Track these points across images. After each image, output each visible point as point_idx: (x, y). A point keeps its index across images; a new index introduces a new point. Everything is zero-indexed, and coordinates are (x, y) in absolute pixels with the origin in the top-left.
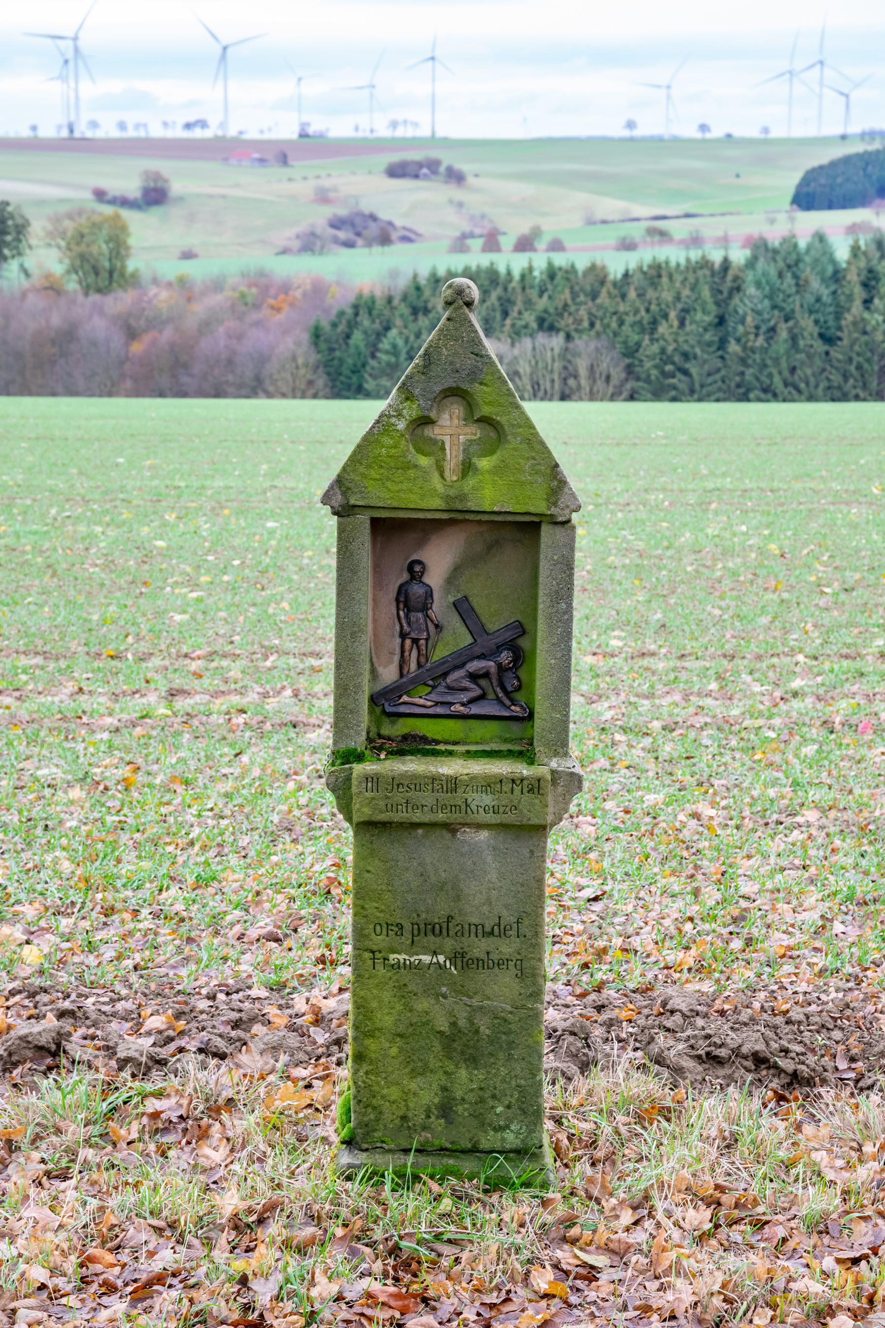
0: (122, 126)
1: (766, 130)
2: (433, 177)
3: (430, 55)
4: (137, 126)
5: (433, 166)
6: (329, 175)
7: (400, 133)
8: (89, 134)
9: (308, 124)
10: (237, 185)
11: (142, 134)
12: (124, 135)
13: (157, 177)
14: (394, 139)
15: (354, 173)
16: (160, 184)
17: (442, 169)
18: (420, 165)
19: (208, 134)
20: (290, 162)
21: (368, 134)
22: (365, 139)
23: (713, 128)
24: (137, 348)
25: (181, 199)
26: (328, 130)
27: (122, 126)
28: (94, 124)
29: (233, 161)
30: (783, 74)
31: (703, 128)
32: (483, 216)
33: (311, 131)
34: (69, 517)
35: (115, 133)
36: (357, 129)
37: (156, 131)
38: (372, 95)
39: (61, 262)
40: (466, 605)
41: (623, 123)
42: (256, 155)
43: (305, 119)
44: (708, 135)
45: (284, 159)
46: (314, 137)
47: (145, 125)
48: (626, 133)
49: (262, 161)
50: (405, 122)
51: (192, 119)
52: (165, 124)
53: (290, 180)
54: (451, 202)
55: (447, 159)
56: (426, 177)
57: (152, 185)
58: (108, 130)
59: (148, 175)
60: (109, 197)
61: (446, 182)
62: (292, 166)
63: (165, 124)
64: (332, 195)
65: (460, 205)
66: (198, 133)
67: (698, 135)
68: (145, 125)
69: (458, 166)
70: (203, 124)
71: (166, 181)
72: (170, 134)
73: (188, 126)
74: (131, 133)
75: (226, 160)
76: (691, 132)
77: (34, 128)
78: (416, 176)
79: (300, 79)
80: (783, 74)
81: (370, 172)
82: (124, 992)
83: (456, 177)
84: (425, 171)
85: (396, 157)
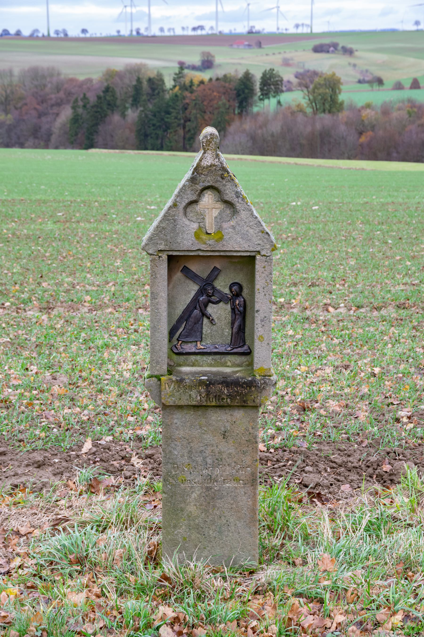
0: (162, 30)
1: (118, 32)
2: (336, 52)
4: (169, 30)
5: (335, 46)
6: (285, 52)
7: (300, 30)
8: (145, 34)
9: (254, 27)
10: (243, 58)
11: (172, 34)
12: (163, 34)
13: (208, 54)
14: (297, 34)
15: (296, 51)
16: (210, 58)
17: (339, 48)
18: (329, 46)
19: (204, 32)
20: (263, 46)
21: (284, 32)
22: (282, 34)
23: (89, 30)
24: (363, 139)
25: (220, 65)
26: (263, 29)
27: (162, 30)
29: (235, 46)
32: (367, 71)
35: (158, 33)
37: (179, 32)
38: (278, 10)
39: (304, 98)
40: (216, 273)
41: (413, 22)
42: (246, 43)
43: (252, 24)
45: (259, 45)
47: (173, 29)
48: (82, 35)
49: (249, 46)
50: (303, 25)
51: (196, 25)
52: (183, 28)
53: (267, 55)
54: (350, 64)
55: (342, 42)
56: (333, 52)
57: (206, 59)
58: (155, 31)
59: (203, 54)
61: (344, 54)
62: (263, 48)
63: (183, 28)
64: (291, 62)
65: (355, 65)
66: (199, 32)
67: (414, 28)
68: (173, 29)
69: (349, 46)
70: (201, 28)
71: (213, 57)
72: (185, 33)
73: (194, 29)
74: (167, 33)
75: (231, 45)
77: (417, 23)
78: (328, 52)
81: (304, 50)
82: (38, 503)
84: (332, 49)
85: (317, 42)
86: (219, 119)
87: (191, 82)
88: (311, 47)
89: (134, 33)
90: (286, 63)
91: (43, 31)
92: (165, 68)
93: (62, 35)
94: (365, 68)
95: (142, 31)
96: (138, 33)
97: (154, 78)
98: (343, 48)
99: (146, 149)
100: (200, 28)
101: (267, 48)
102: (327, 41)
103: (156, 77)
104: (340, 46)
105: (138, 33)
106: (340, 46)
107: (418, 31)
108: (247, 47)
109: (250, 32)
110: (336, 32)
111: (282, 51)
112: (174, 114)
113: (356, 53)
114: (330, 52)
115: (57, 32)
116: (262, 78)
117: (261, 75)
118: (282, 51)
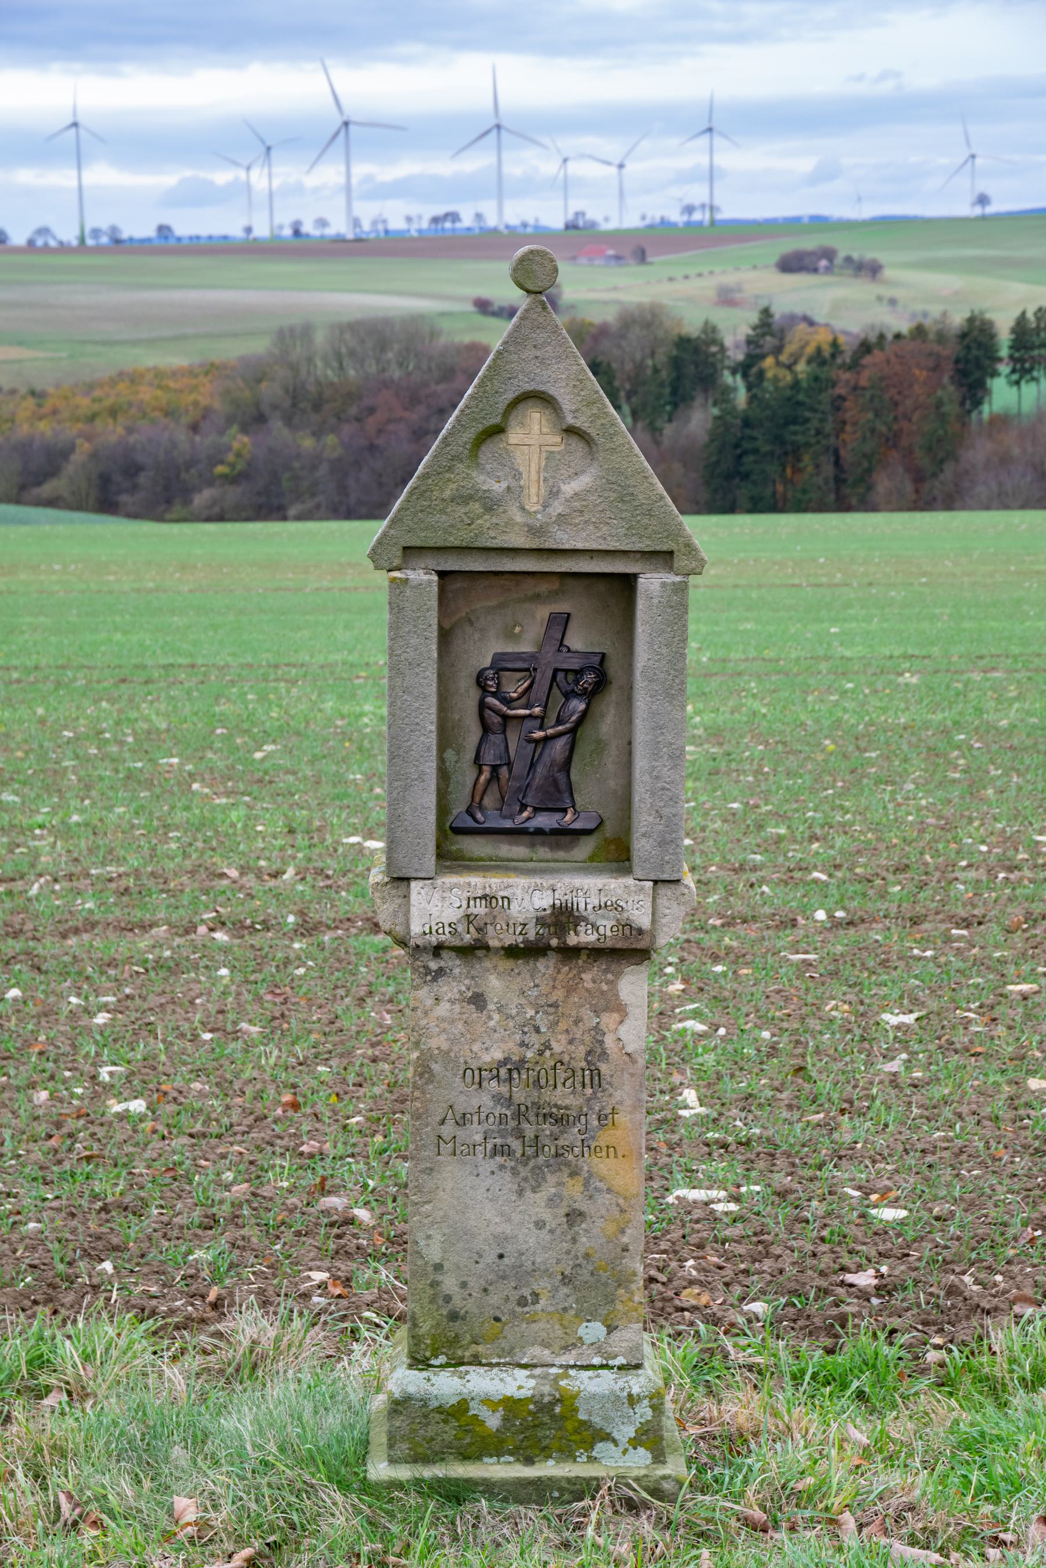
1: (249, 230)
3: (706, 126)
5: (829, 254)
6: (711, 273)
8: (316, 232)
9: (583, 214)
10: (615, 289)
17: (839, 260)
20: (649, 259)
28: (322, 223)
29: (583, 260)
30: (487, 133)
31: (983, 200)
33: (125, 235)
34: (788, 774)
36: (643, 218)
42: (611, 252)
44: (990, 210)
45: (641, 256)
46: (584, 228)
49: (618, 258)
53: (671, 279)
54: (880, 299)
55: (845, 247)
60: (495, 307)
61: (856, 276)
62: (651, 263)
64: (738, 296)
65: (893, 302)
67: (978, 211)
69: (869, 255)
70: (454, 217)
76: (965, 209)
78: (815, 270)
79: (565, 160)
80: (487, 133)
81: (755, 267)
83: (872, 270)
86: (941, 432)
87: (835, 344)
88: (774, 259)
89: (288, 232)
90: (727, 298)
91: (69, 235)
92: (443, 314)
93: (104, 240)
94: (919, 307)
95: (308, 228)
96: (297, 233)
97: (698, 338)
98: (848, 259)
99: (730, 509)
100: (450, 218)
101: (661, 265)
102: (809, 244)
103: (703, 336)
104: (842, 254)
105: (297, 233)
106: (842, 254)
107: (984, 218)
108: (613, 262)
109: (570, 226)
110: (754, 223)
111: (692, 271)
112: (815, 423)
113: (888, 273)
114: (821, 270)
115: (96, 233)
116: (1013, 331)
117: (1011, 323)
118: (705, 270)
